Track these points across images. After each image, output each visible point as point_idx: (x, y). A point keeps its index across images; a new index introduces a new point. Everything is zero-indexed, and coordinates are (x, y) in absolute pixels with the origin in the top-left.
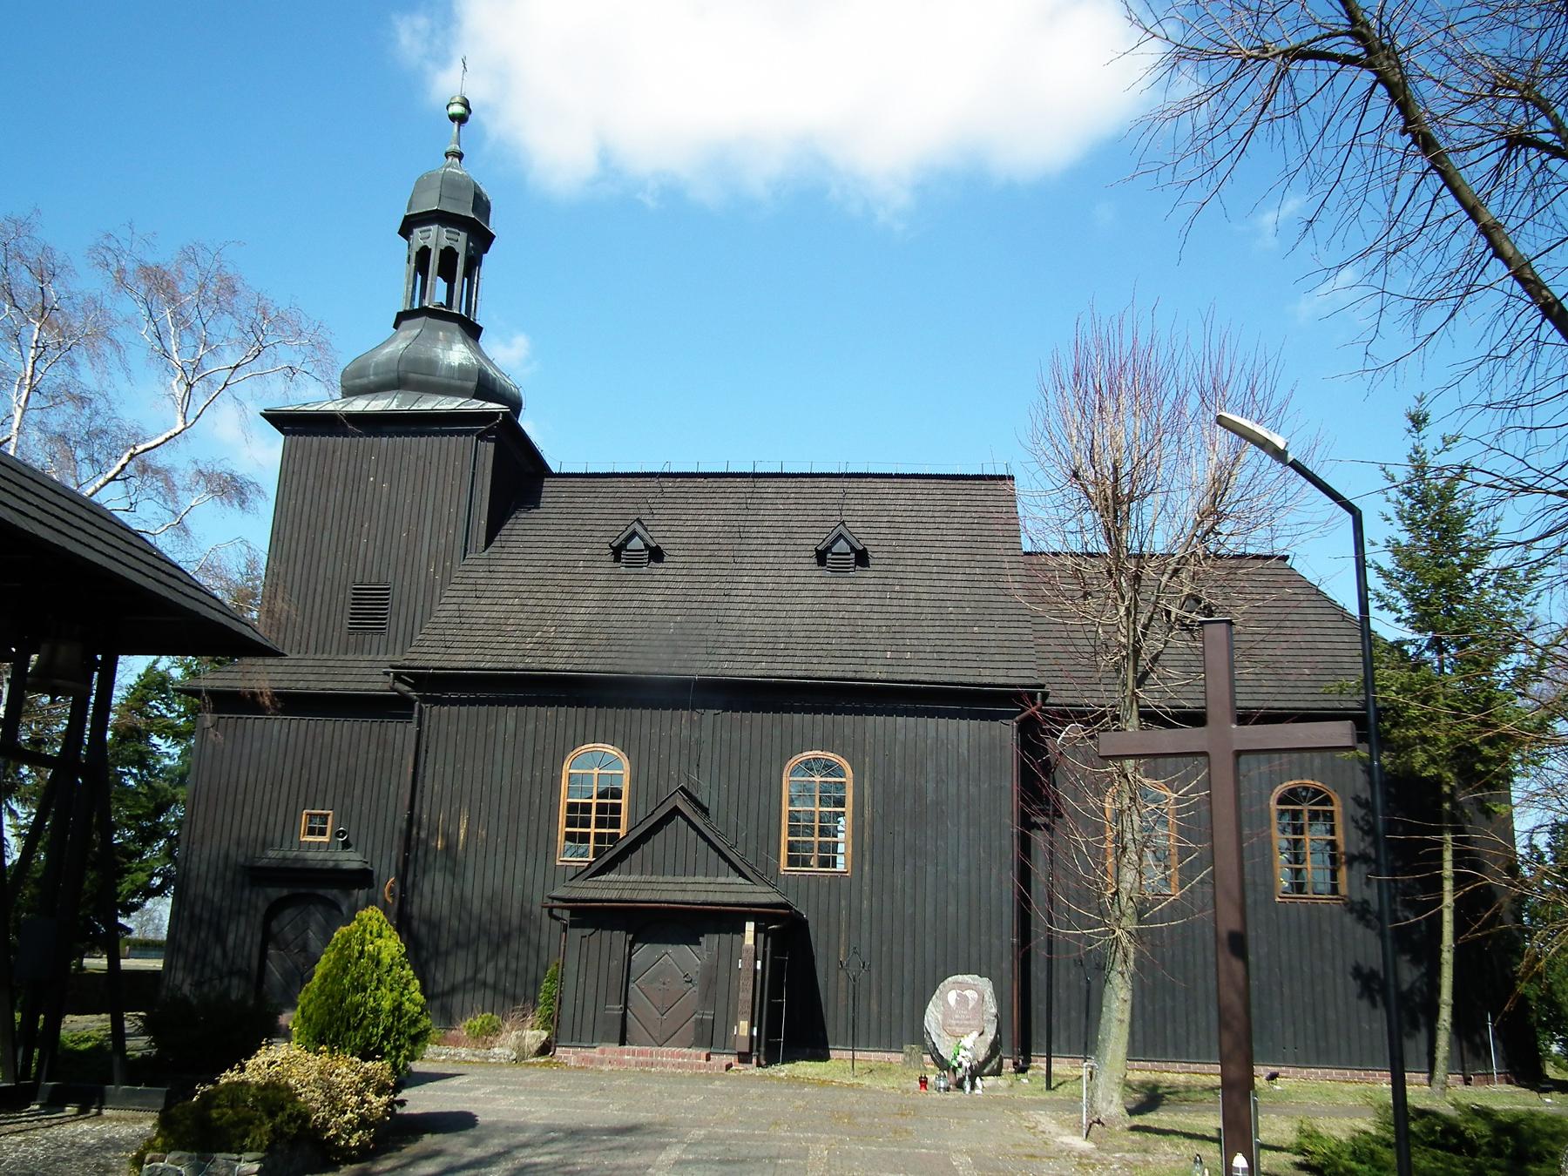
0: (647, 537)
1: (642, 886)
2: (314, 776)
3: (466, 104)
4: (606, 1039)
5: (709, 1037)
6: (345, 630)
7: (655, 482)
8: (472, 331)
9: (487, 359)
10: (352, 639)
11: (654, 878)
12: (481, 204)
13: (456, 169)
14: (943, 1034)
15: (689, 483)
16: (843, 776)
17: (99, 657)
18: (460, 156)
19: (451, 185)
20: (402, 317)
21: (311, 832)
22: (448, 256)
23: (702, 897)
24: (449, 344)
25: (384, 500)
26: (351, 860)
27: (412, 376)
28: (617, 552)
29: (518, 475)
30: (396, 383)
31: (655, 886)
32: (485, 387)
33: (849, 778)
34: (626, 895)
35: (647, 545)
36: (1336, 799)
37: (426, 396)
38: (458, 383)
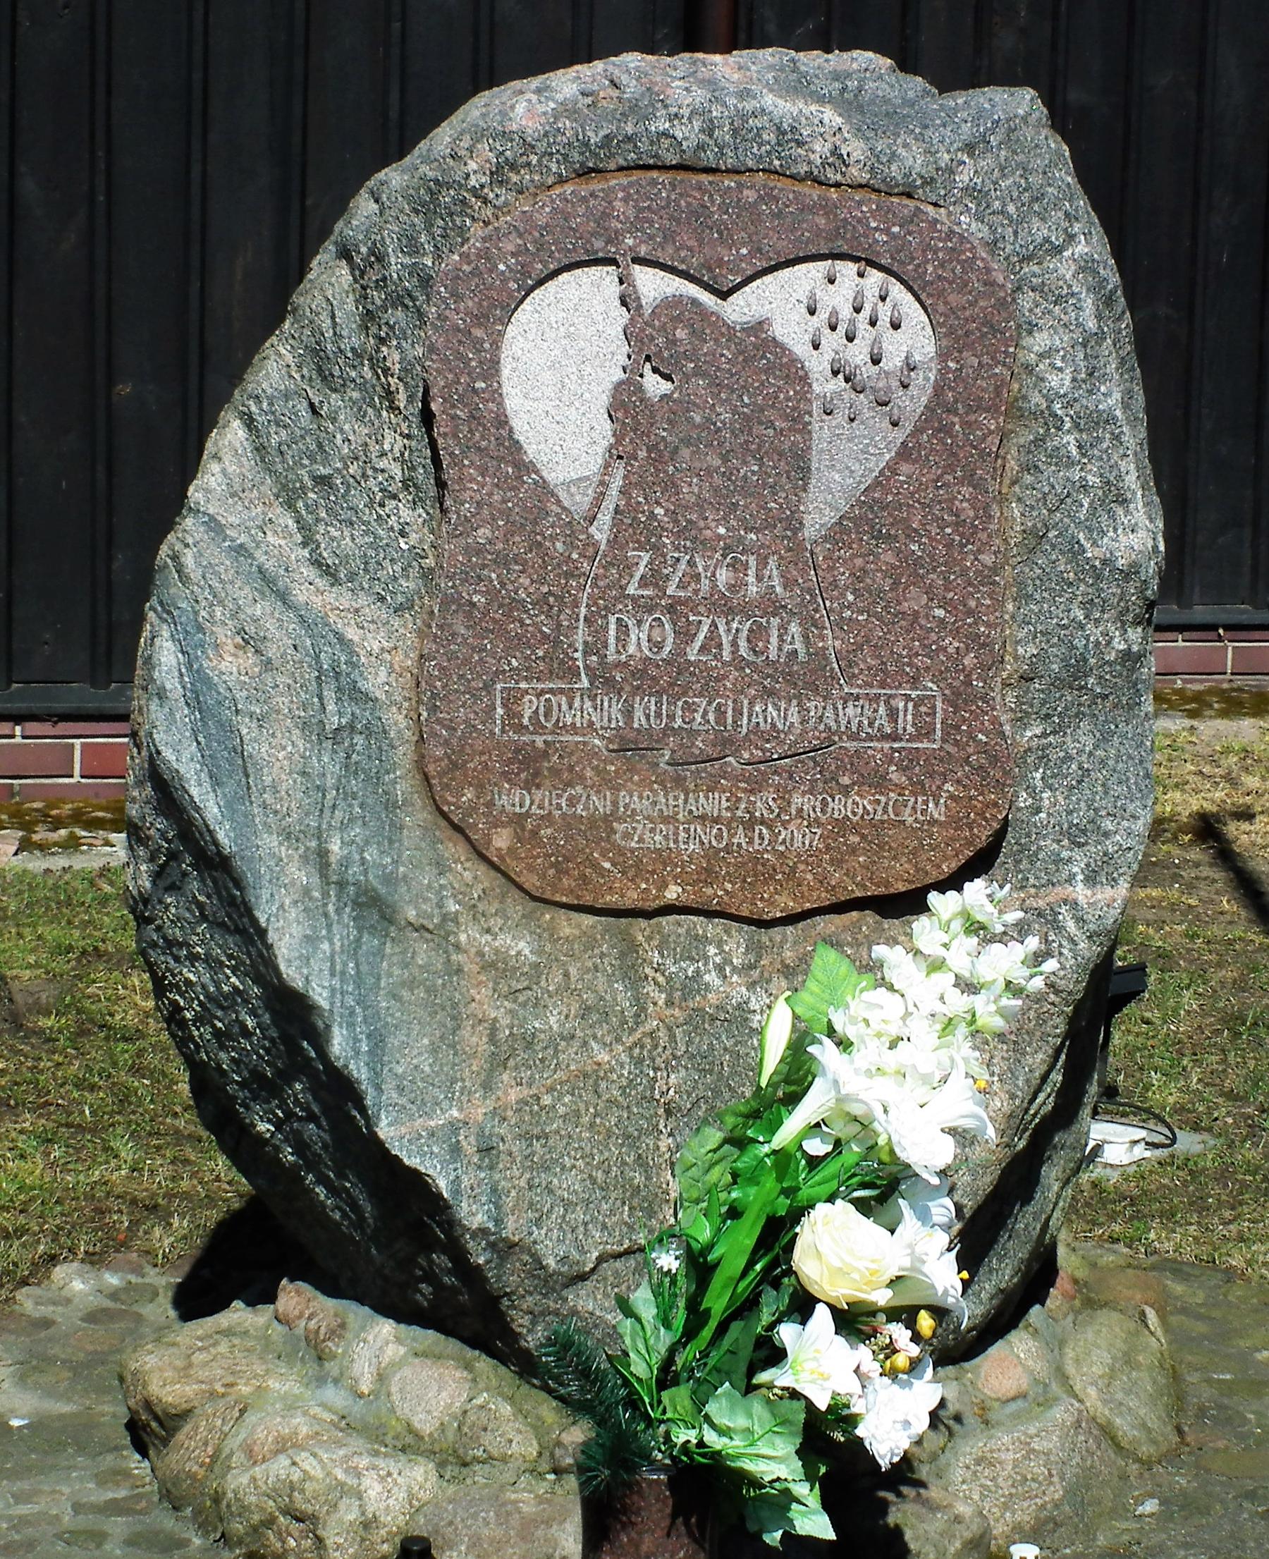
14: (434, 880)
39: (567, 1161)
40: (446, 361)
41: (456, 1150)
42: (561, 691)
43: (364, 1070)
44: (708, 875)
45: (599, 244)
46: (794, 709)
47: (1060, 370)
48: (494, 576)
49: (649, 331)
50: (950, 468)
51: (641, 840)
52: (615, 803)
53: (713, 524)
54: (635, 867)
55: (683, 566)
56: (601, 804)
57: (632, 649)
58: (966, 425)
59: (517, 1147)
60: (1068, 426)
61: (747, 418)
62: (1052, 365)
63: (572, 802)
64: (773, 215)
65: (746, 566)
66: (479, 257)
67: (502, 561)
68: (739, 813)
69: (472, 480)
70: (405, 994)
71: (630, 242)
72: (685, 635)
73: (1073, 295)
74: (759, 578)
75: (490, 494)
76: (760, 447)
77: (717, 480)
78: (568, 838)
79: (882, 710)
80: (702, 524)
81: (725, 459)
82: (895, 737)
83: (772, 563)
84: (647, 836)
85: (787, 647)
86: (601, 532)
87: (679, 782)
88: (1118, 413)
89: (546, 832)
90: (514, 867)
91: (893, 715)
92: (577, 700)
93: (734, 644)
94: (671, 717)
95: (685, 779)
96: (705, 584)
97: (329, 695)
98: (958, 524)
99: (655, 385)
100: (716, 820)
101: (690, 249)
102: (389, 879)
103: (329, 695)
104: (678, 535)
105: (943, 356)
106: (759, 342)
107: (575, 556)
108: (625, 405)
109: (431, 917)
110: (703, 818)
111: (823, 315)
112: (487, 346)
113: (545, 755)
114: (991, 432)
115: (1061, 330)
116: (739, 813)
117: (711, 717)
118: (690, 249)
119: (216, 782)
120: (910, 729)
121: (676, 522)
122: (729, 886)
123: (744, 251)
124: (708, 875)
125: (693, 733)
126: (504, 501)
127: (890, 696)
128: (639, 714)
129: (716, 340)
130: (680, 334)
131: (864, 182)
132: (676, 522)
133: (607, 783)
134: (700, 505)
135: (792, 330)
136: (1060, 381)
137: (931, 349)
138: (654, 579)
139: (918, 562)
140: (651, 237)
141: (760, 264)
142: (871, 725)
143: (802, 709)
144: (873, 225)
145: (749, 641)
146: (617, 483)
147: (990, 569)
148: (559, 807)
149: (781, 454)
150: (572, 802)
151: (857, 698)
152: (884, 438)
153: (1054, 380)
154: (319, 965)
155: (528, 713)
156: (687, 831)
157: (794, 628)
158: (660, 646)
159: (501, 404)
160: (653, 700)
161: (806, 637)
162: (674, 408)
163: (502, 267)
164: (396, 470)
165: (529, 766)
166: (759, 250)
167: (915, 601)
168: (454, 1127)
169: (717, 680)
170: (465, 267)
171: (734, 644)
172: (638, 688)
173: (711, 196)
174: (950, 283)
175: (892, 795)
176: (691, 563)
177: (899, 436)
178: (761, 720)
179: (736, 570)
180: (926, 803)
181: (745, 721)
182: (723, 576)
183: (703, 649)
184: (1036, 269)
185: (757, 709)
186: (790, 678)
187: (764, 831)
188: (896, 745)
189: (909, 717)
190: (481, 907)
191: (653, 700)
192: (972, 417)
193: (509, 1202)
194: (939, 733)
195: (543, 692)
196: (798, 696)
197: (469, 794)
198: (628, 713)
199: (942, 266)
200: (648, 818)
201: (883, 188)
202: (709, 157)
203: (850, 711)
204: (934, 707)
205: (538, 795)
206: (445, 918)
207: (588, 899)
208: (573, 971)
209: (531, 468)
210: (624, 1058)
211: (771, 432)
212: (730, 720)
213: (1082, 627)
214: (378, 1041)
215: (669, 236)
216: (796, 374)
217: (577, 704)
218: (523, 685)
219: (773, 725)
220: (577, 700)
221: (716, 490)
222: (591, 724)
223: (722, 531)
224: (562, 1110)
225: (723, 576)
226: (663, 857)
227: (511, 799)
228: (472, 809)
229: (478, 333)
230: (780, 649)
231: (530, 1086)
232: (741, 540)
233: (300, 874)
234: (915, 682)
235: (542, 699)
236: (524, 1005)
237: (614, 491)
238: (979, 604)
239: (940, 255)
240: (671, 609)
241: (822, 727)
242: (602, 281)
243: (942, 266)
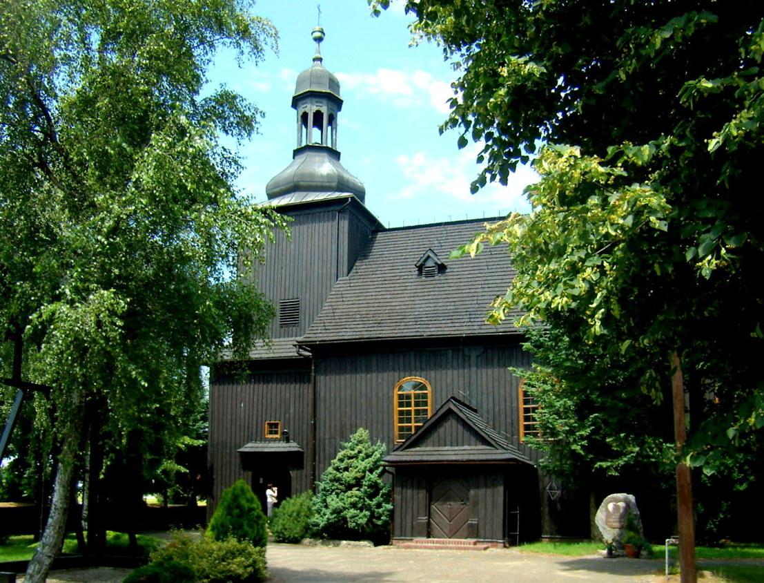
0: (436, 259)
1: (435, 453)
2: (269, 403)
3: (322, 32)
4: (420, 535)
5: (474, 532)
6: (278, 326)
7: (442, 228)
8: (335, 154)
9: (343, 168)
10: (282, 329)
11: (440, 448)
12: (334, 83)
13: (318, 67)
14: (606, 527)
15: (462, 226)
16: (426, 390)
17: (585, 122)
18: (320, 59)
19: (313, 77)
20: (297, 152)
21: (271, 433)
22: (318, 117)
23: (466, 458)
24: (322, 163)
25: (292, 253)
26: (293, 446)
27: (302, 183)
28: (420, 268)
29: (364, 230)
30: (295, 188)
31: (441, 453)
32: (342, 185)
33: (429, 391)
34: (425, 458)
35: (436, 263)
36: (429, 387)
37: (310, 194)
38: (327, 184)
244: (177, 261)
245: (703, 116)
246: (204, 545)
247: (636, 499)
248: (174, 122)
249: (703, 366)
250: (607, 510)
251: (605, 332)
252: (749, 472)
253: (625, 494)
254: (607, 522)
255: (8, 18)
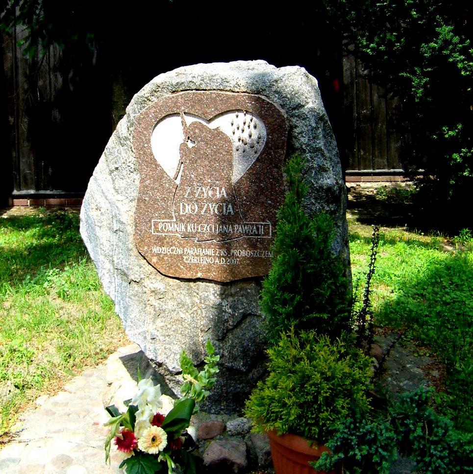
14: (138, 269)
39: (175, 343)
40: (137, 139)
41: (145, 338)
42: (169, 222)
43: (123, 316)
44: (209, 270)
45: (175, 109)
46: (230, 227)
47: (304, 137)
48: (151, 193)
49: (188, 130)
50: (271, 164)
51: (191, 261)
52: (183, 251)
53: (207, 179)
54: (189, 268)
55: (199, 190)
56: (180, 251)
57: (187, 211)
58: (275, 153)
59: (162, 338)
60: (307, 152)
61: (215, 152)
62: (303, 136)
63: (172, 251)
64: (220, 100)
65: (216, 190)
66: (145, 114)
67: (153, 189)
68: (217, 254)
69: (144, 169)
70: (133, 297)
71: (183, 108)
72: (200, 208)
73: (308, 118)
74: (220, 193)
75: (149, 172)
76: (219, 159)
77: (207, 168)
78: (172, 260)
79: (255, 228)
80: (204, 179)
81: (210, 162)
82: (258, 235)
83: (223, 189)
84: (192, 260)
85: (228, 211)
86: (178, 182)
87: (200, 246)
88: (323, 148)
89: (166, 258)
90: (158, 267)
91: (258, 229)
92: (173, 224)
93: (214, 210)
94: (198, 229)
95: (201, 245)
96: (205, 195)
97: (114, 222)
98: (274, 179)
99: (190, 145)
100: (210, 256)
101: (198, 110)
102: (128, 269)
103: (114, 222)
104: (198, 182)
105: (268, 135)
106: (218, 133)
107: (171, 188)
108: (183, 148)
109: (138, 279)
110: (207, 255)
111: (235, 126)
112: (147, 135)
113: (165, 238)
114: (282, 154)
115: (305, 127)
116: (217, 254)
117: (208, 229)
118: (198, 110)
119: (91, 243)
120: (263, 233)
121: (197, 179)
122: (215, 273)
123: (213, 110)
124: (209, 270)
125: (203, 233)
126: (153, 174)
127: (257, 224)
128: (189, 228)
129: (206, 133)
130: (197, 131)
131: (245, 91)
132: (197, 179)
133: (181, 246)
134: (204, 174)
135: (227, 130)
136: (304, 140)
137: (265, 133)
138: (192, 193)
139: (263, 189)
140: (189, 107)
141: (217, 113)
142: (252, 231)
143: (233, 228)
144: (247, 102)
145: (218, 209)
146: (182, 169)
147: (283, 190)
148: (169, 252)
149: (225, 161)
150: (172, 251)
151: (248, 224)
152: (253, 156)
153: (302, 139)
154: (112, 288)
155: (160, 228)
156: (203, 259)
157: (230, 206)
158: (194, 210)
159: (151, 150)
160: (193, 224)
161: (233, 208)
162: (196, 150)
163: (151, 116)
164: (133, 166)
165: (161, 241)
166: (217, 109)
167: (263, 199)
168: (145, 332)
169: (210, 219)
170: (141, 116)
171: (214, 210)
172: (189, 221)
173: (204, 96)
174: (269, 116)
175: (258, 250)
176: (202, 189)
177: (257, 155)
178: (222, 230)
179: (213, 191)
180: (268, 252)
181: (217, 230)
182: (210, 193)
183: (206, 212)
184: (297, 111)
185: (221, 227)
186: (229, 219)
187: (224, 259)
188: (259, 237)
189: (262, 230)
190: (150, 277)
191: (193, 224)
192: (276, 151)
193: (159, 352)
194: (271, 234)
195: (164, 222)
196: (232, 224)
197: (146, 248)
198: (186, 228)
199: (266, 111)
200: (192, 255)
201: (251, 92)
202: (203, 87)
203: (246, 228)
204: (269, 227)
205: (163, 248)
206: (141, 279)
207: (177, 276)
208: (174, 294)
209: (159, 166)
210: (189, 317)
211: (222, 155)
212: (213, 230)
213: (314, 205)
214: (126, 309)
215: (193, 106)
216: (227, 140)
217: (173, 225)
218: (159, 220)
219: (225, 231)
220: (173, 224)
221: (208, 171)
222: (177, 231)
223: (209, 181)
224: (173, 329)
225: (210, 193)
226: (197, 265)
227: (156, 249)
228: (147, 252)
229: (145, 132)
230: (226, 211)
231: (164, 322)
232: (214, 183)
233: (108, 265)
234: (263, 221)
235: (164, 224)
236: (162, 302)
237: (181, 171)
238: (280, 200)
239: (266, 109)
240: (196, 201)
241: (238, 232)
242: (176, 120)
243: (266, 111)
244: (346, 453)
245: (327, 306)
246: (272, 424)
247: (326, 91)
248: (152, 217)
249: (414, 14)
250: (146, 160)
251: (291, 283)
252: (358, 421)
253: (260, 66)
254: (145, 241)
255: (224, 316)
